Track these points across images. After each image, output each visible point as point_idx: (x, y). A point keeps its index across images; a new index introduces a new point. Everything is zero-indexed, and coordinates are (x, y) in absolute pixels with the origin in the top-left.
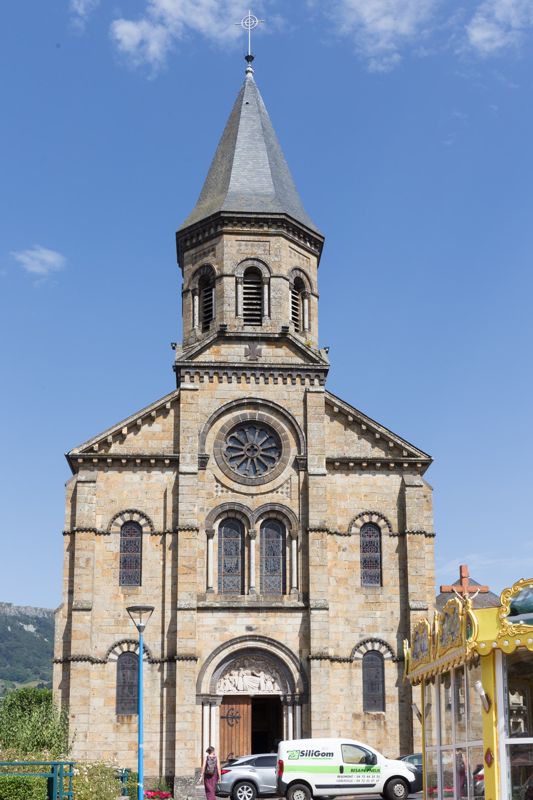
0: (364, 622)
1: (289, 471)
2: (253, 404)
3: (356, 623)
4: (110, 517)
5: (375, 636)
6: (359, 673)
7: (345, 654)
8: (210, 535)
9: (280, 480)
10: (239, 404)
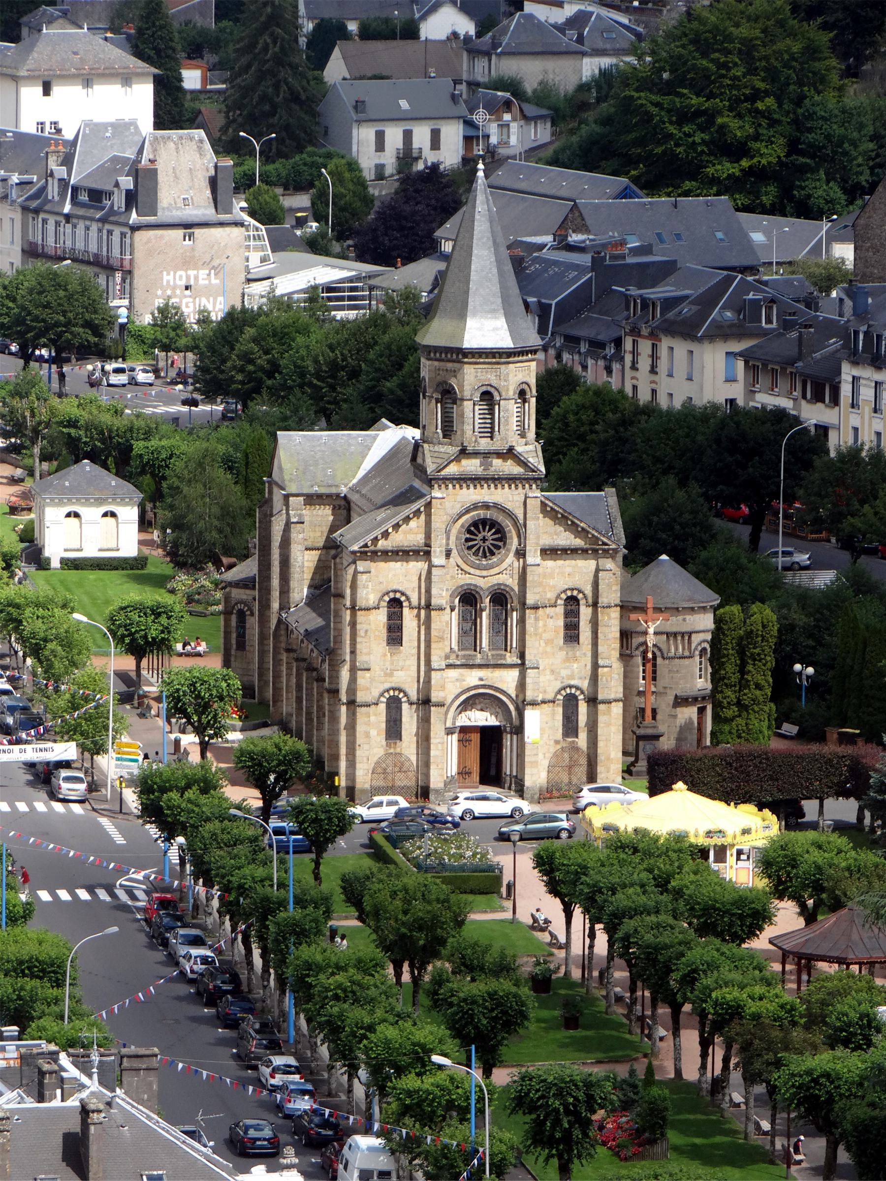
0: (564, 673)
1: (511, 558)
2: (486, 506)
3: (559, 673)
4: (380, 595)
5: (572, 683)
6: (560, 710)
7: (550, 696)
8: (452, 610)
9: (505, 565)
10: (475, 507)
